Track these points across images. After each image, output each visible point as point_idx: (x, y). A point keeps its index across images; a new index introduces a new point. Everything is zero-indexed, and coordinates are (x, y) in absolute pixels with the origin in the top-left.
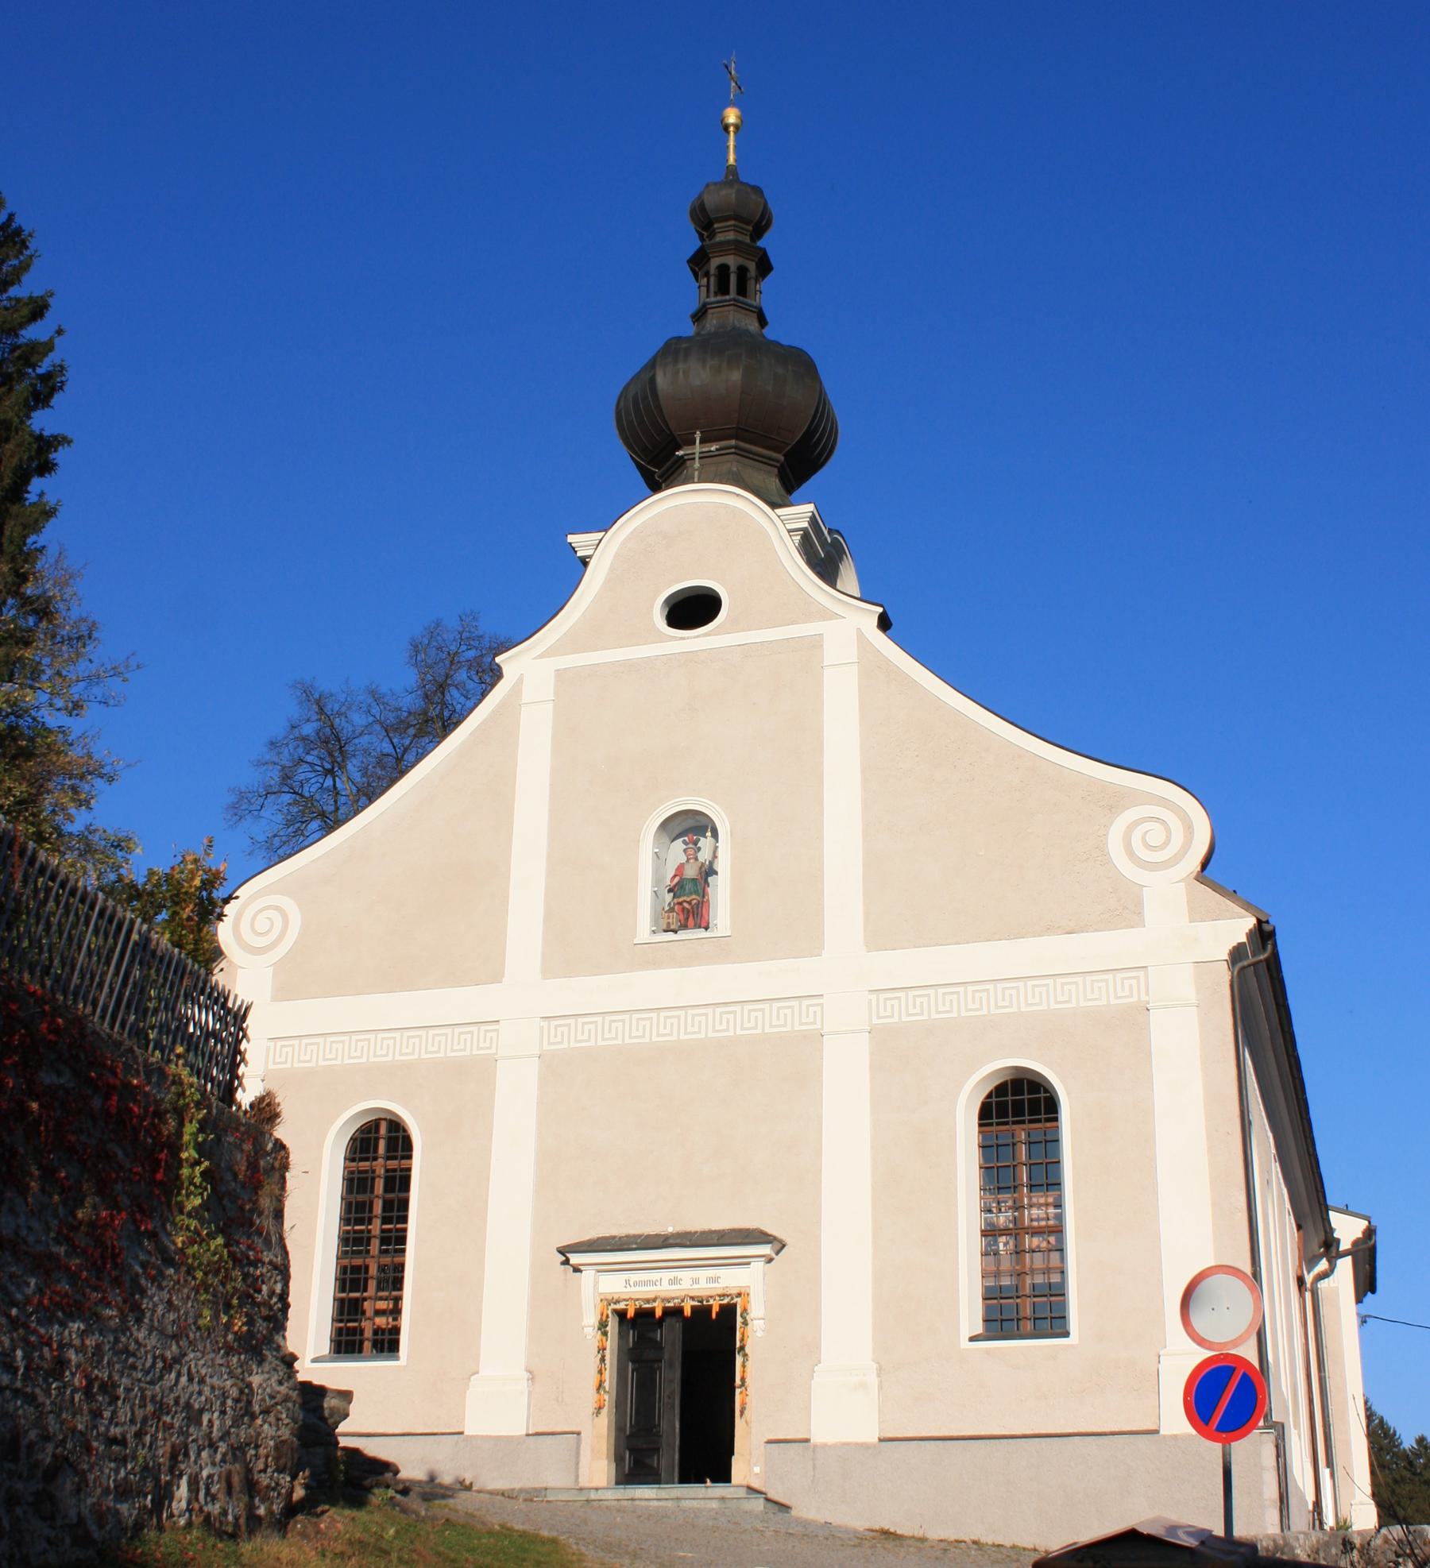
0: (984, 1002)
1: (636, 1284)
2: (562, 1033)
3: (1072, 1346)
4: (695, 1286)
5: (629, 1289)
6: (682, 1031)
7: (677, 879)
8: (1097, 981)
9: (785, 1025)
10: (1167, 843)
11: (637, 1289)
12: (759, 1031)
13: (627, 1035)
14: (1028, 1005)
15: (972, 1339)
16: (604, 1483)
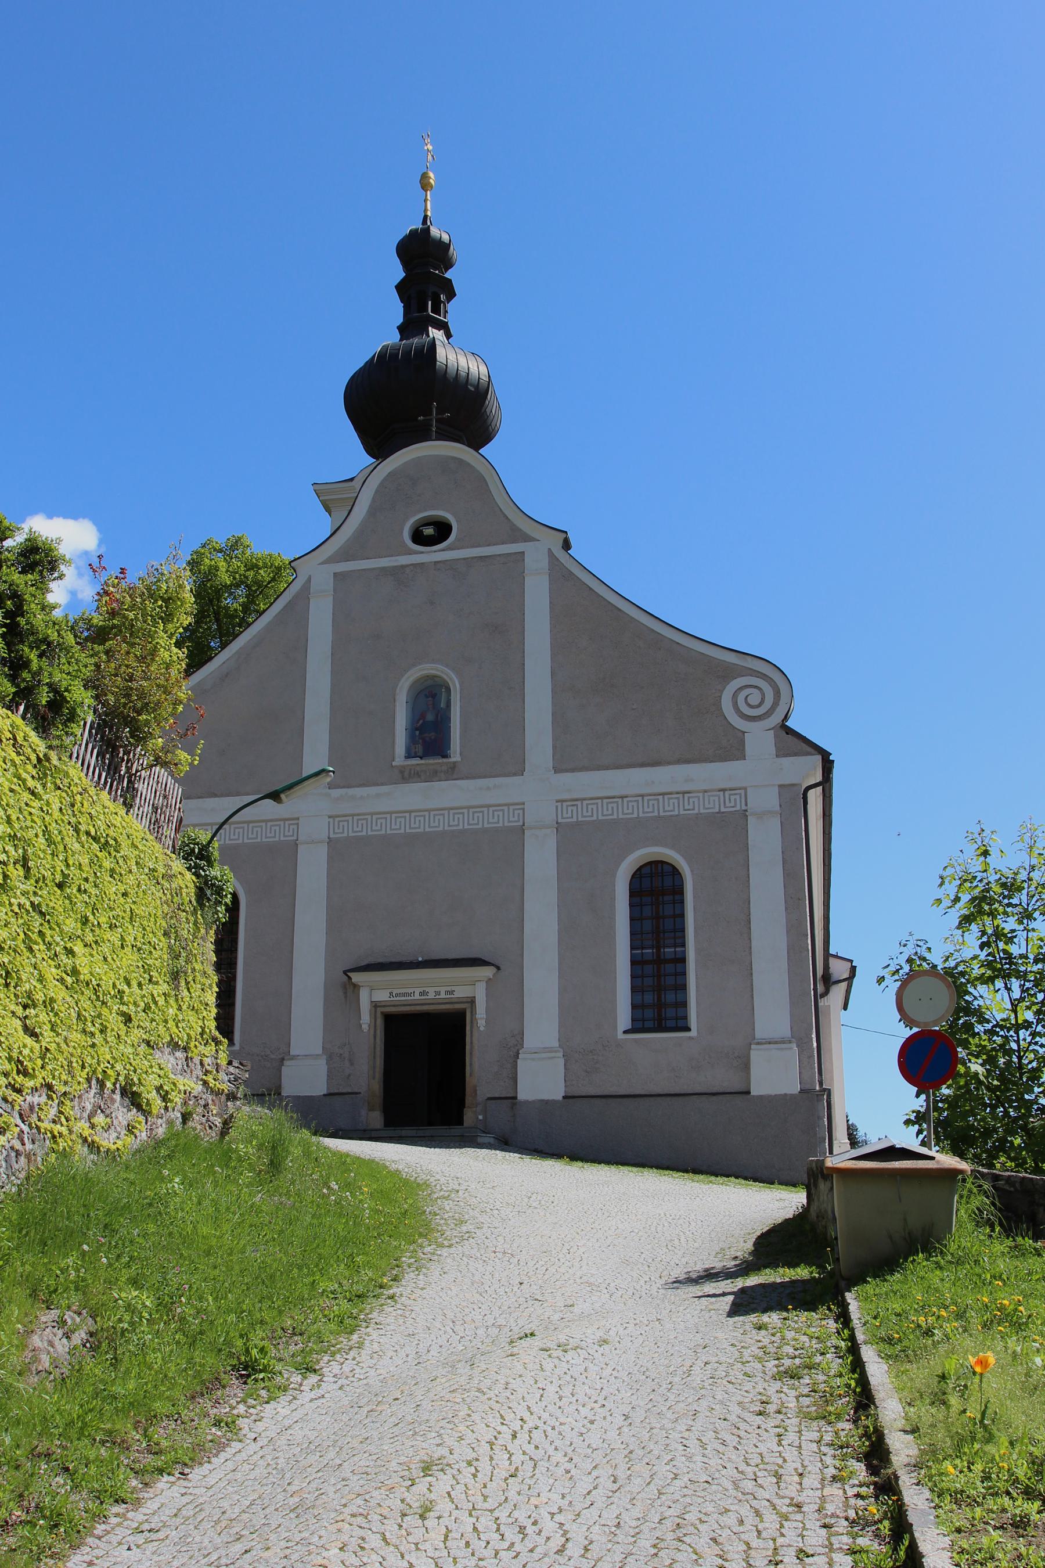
0: (374, 823)
1: (397, 995)
2: (478, 817)
3: (690, 1038)
4: (437, 997)
5: (392, 999)
6: (369, 829)
7: (421, 722)
8: (713, 796)
9: (612, 814)
10: (759, 706)
11: (398, 998)
12: (480, 826)
13: (407, 826)
14: (354, 832)
15: (625, 1032)
16: (379, 1127)
